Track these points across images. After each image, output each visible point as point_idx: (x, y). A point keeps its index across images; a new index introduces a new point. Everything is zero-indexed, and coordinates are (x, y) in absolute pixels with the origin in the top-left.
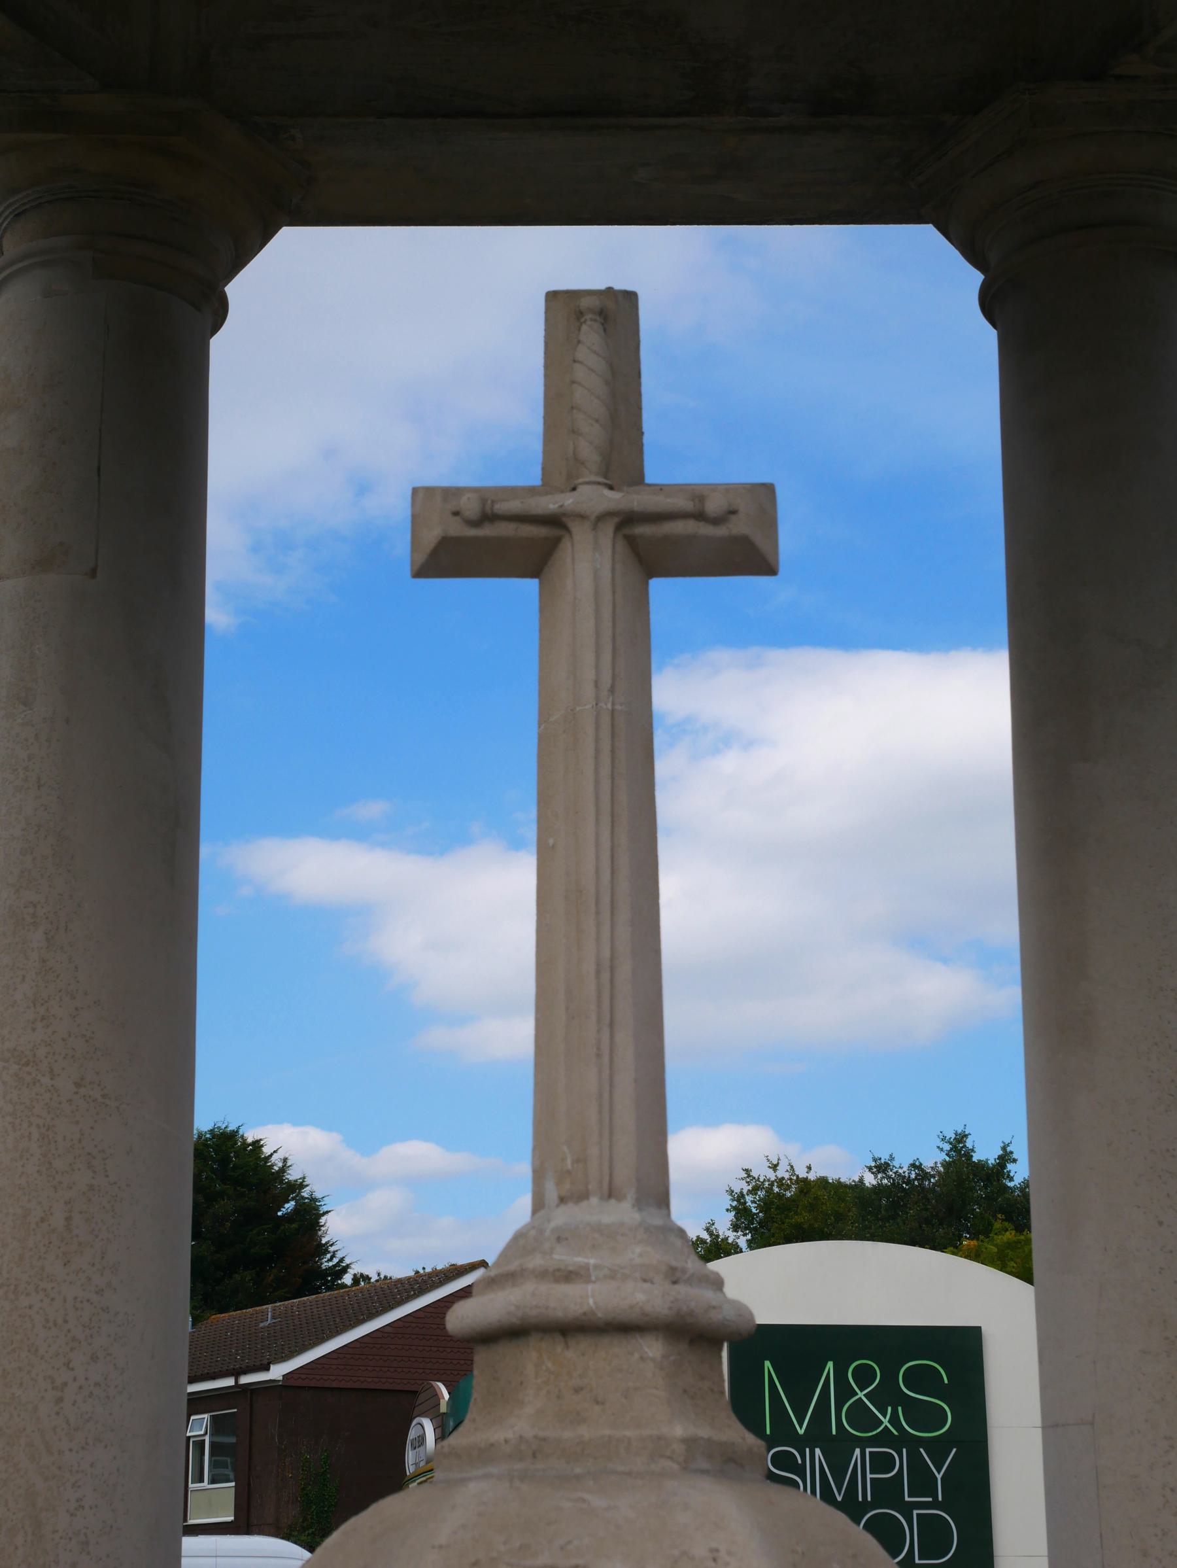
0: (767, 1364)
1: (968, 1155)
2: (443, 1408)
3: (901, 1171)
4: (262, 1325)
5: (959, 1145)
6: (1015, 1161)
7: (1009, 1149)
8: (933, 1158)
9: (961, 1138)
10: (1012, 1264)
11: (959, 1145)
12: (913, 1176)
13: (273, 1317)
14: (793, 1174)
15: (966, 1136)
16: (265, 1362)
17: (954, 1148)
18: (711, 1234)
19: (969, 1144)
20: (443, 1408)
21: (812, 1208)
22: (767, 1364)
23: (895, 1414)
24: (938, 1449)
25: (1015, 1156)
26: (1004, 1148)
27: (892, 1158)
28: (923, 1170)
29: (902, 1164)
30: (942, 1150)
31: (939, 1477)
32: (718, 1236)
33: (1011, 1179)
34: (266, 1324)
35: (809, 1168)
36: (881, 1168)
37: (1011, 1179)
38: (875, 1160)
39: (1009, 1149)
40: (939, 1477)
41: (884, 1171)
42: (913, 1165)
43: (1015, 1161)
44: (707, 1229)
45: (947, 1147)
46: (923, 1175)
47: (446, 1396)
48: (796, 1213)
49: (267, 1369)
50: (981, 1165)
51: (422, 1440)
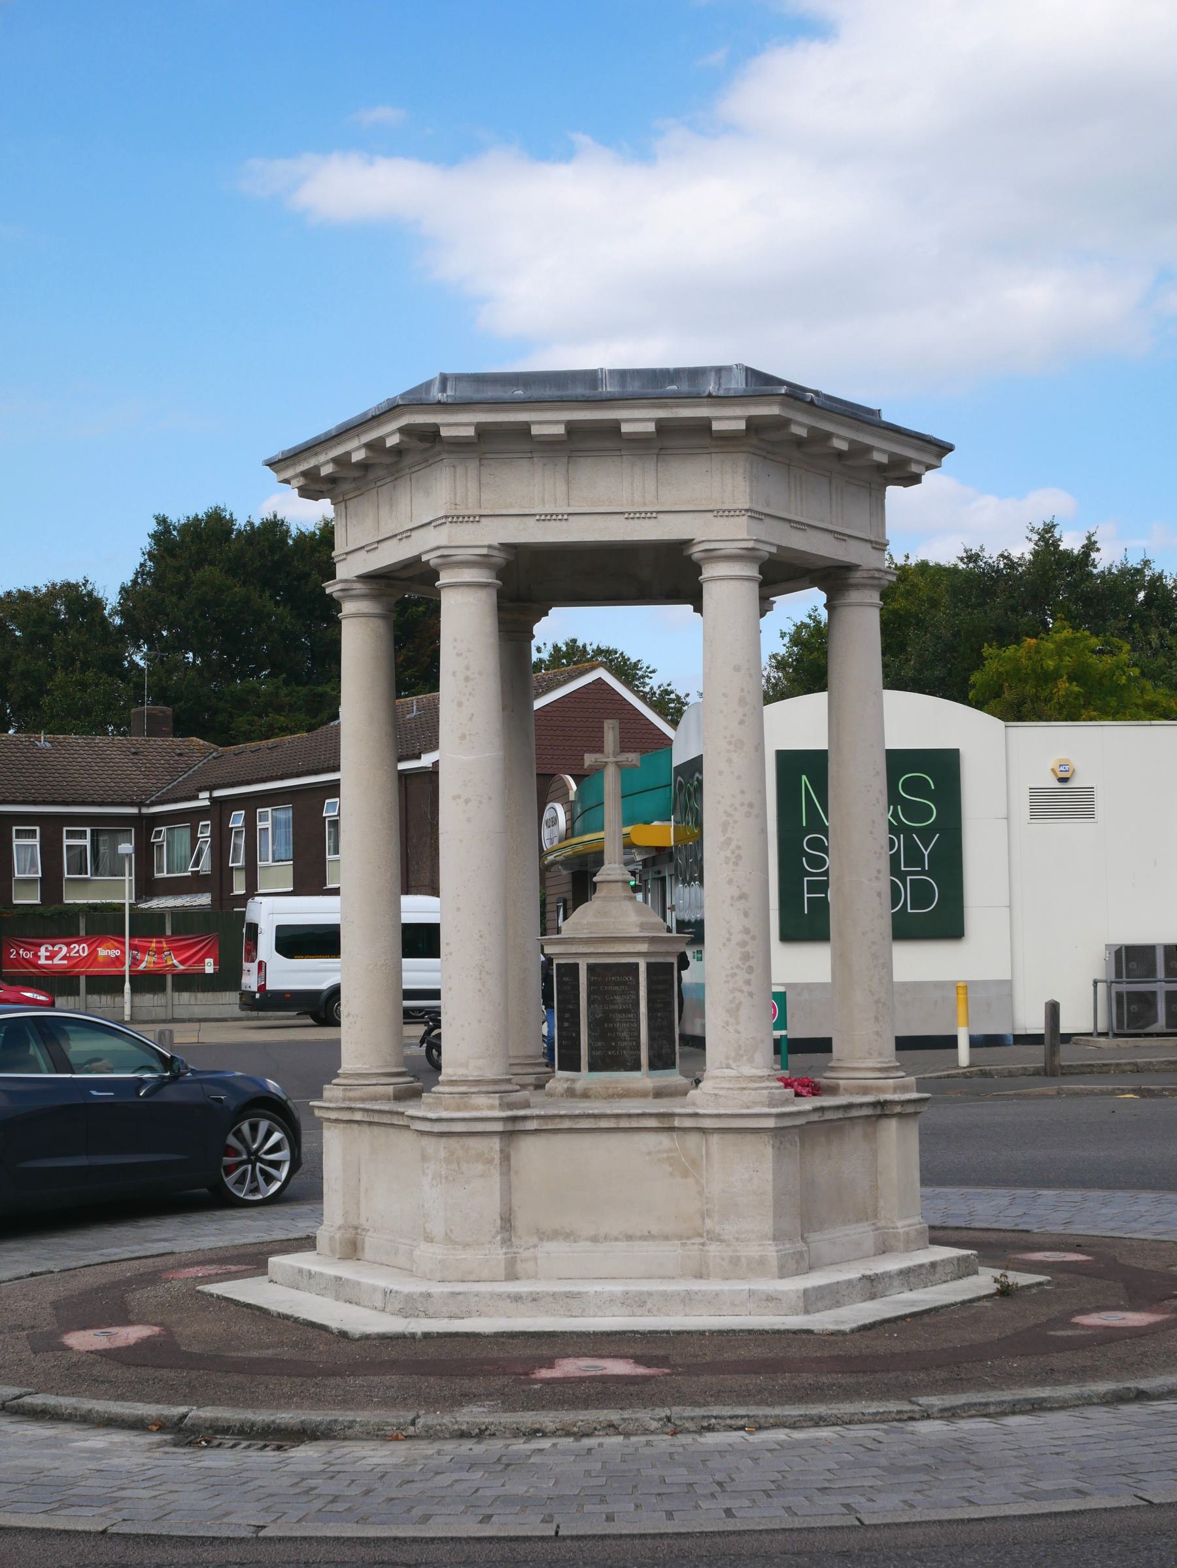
0: (804, 777)
1: (1056, 545)
2: (572, 797)
3: (990, 561)
4: (408, 716)
5: (1047, 537)
6: (1098, 550)
7: (1093, 539)
8: (1023, 549)
9: (1049, 528)
10: (1068, 658)
11: (1047, 537)
12: (1002, 566)
13: (418, 710)
14: (892, 563)
15: (1054, 526)
16: (417, 752)
17: (1042, 538)
18: (814, 620)
19: (1057, 535)
20: (572, 797)
21: (908, 593)
22: (804, 777)
23: (895, 810)
24: (926, 835)
25: (1098, 545)
26: (1089, 538)
27: (982, 549)
28: (1011, 560)
29: (991, 554)
30: (1030, 540)
31: (926, 853)
32: (820, 622)
33: (1095, 567)
34: (412, 715)
35: (907, 557)
36: (973, 558)
37: (1095, 567)
38: (966, 551)
39: (1093, 539)
40: (926, 853)
41: (975, 561)
42: (1002, 555)
43: (1098, 550)
44: (810, 616)
45: (1036, 537)
46: (1011, 565)
47: (574, 787)
48: (894, 600)
49: (418, 757)
50: (1067, 554)
51: (555, 821)
